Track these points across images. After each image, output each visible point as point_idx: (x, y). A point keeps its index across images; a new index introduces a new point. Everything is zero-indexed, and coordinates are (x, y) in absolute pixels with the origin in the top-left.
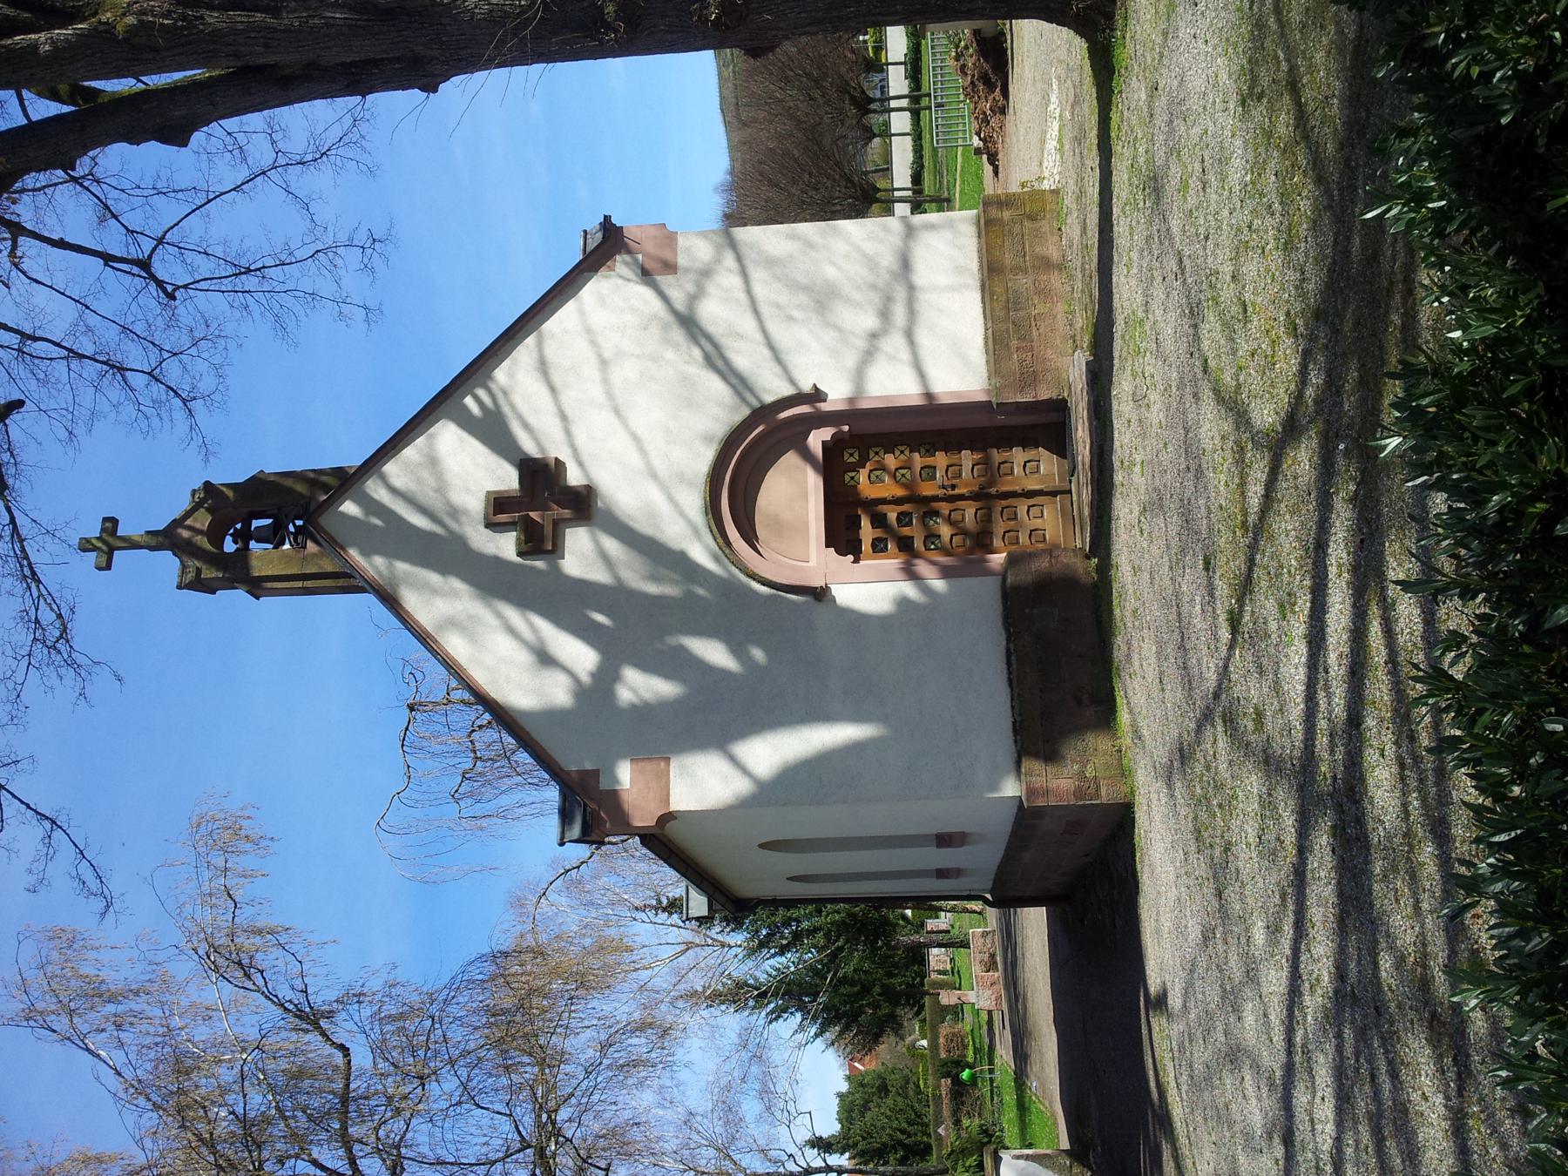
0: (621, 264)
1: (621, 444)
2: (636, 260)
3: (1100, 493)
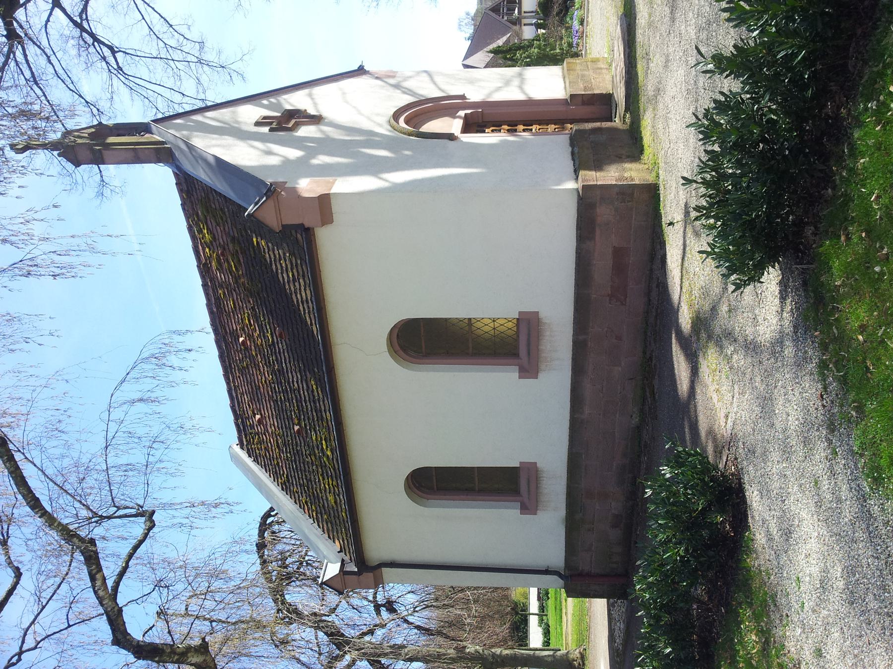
3: (629, 47)
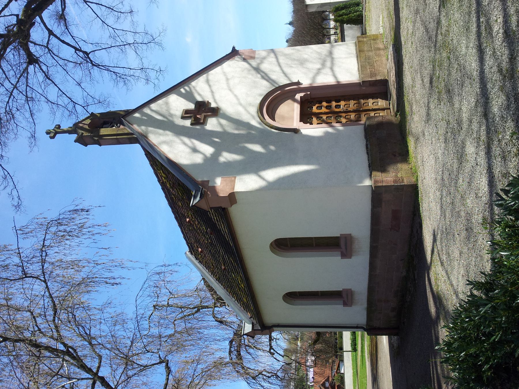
0: (237, 58)
1: (231, 97)
2: (242, 57)
3: (399, 77)
